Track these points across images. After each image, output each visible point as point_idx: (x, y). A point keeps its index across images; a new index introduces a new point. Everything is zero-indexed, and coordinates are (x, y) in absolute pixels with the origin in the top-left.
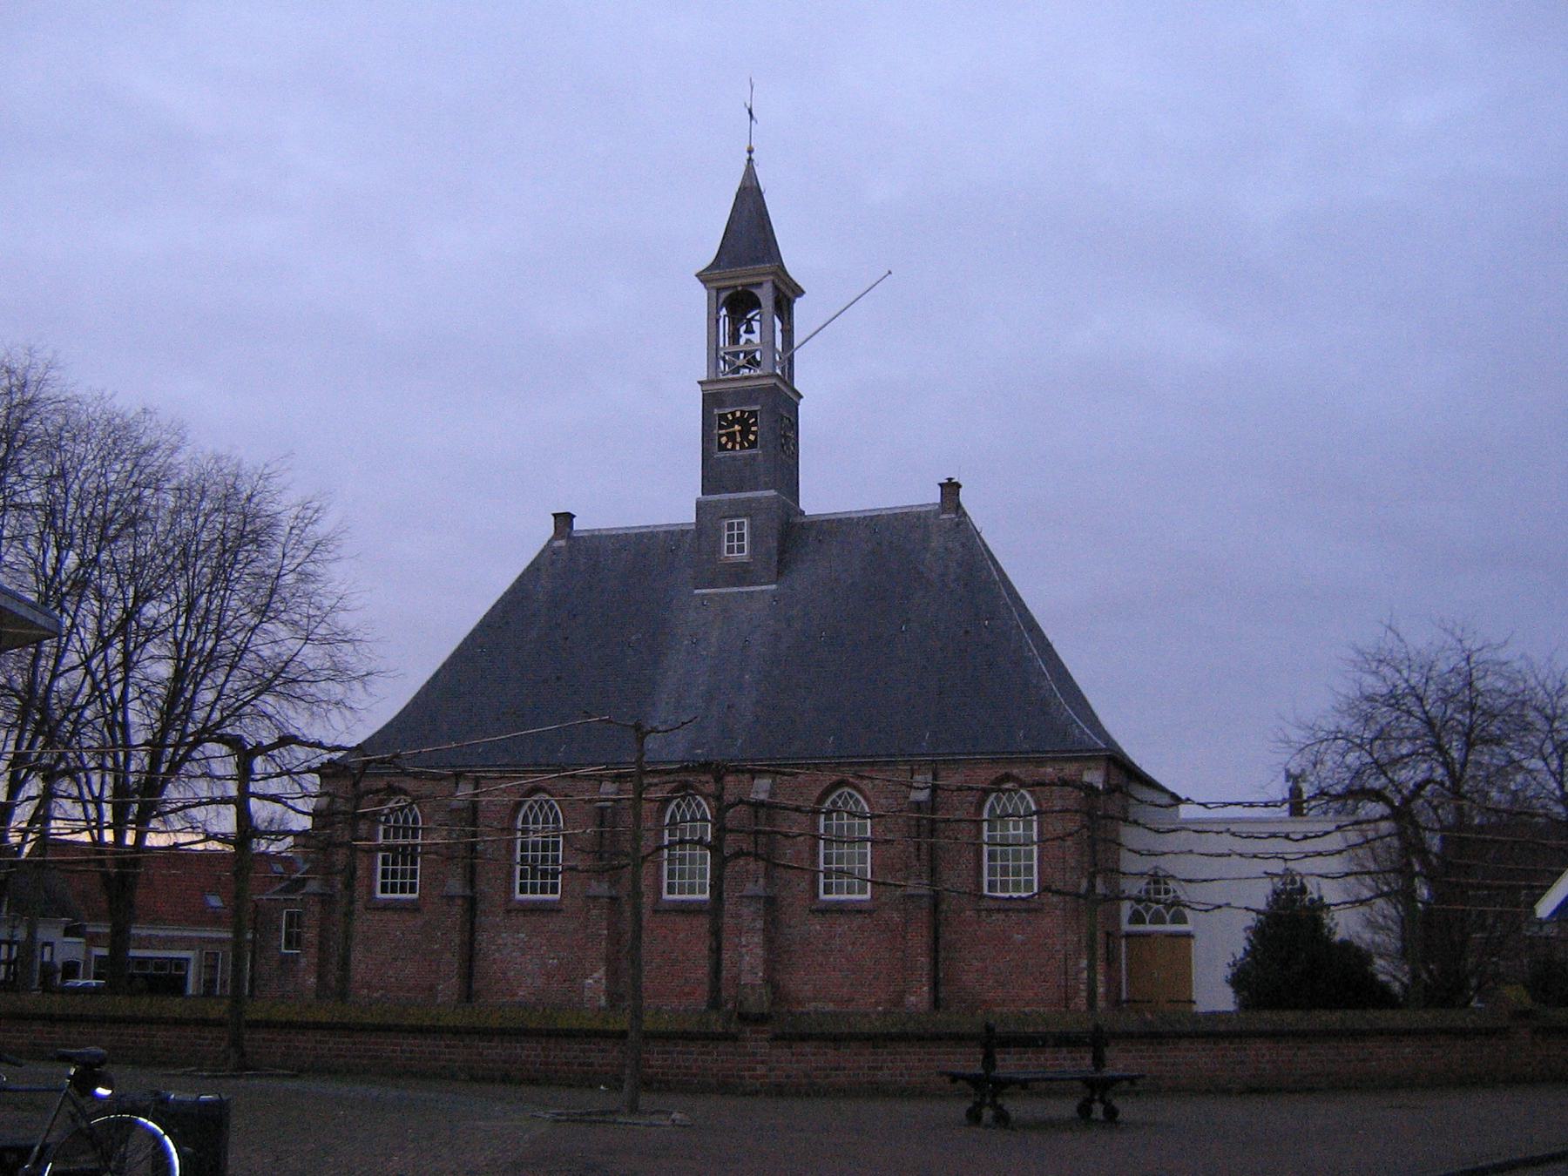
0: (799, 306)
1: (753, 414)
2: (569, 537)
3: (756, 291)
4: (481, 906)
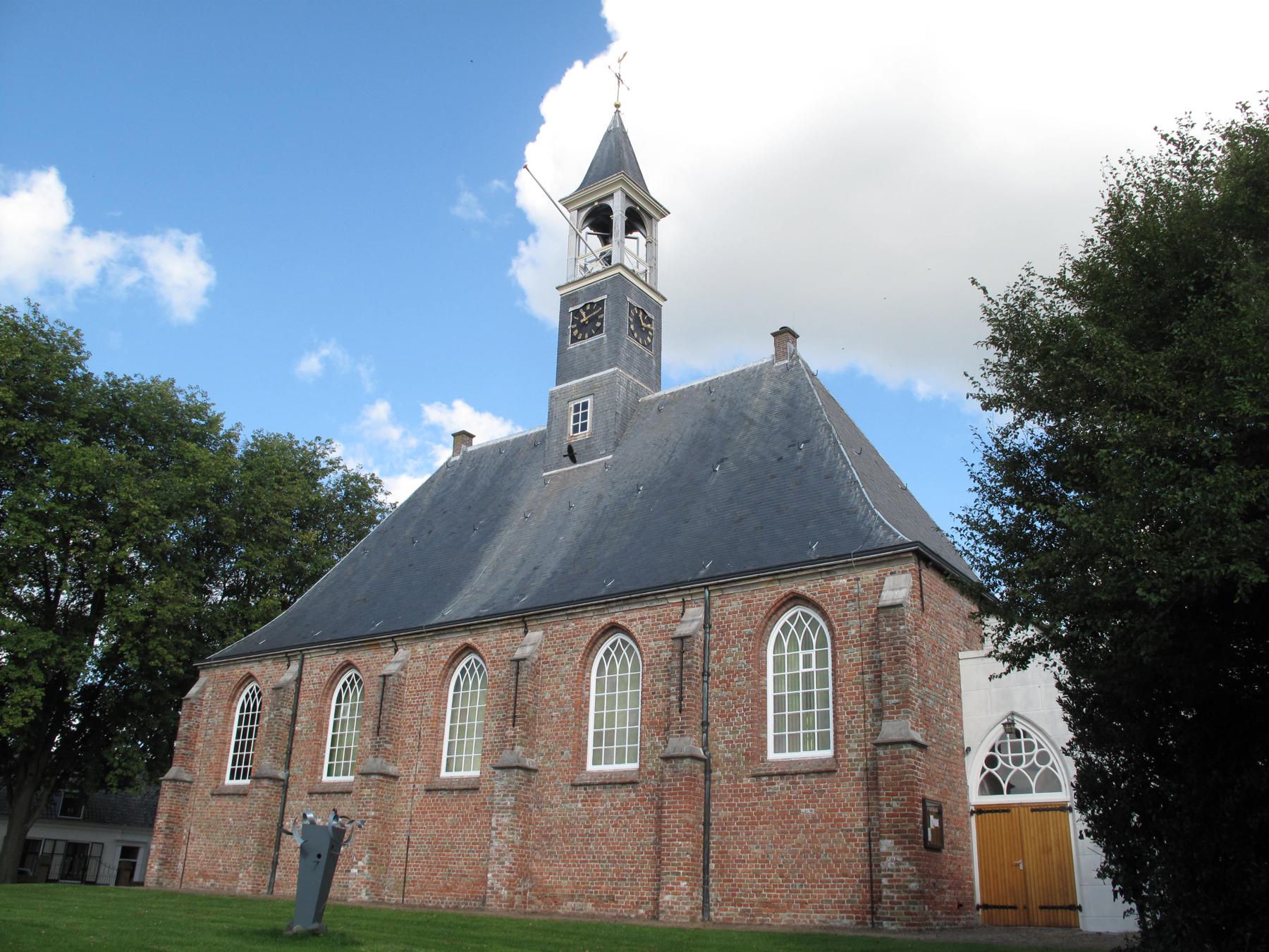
1: (601, 303)
3: (610, 203)
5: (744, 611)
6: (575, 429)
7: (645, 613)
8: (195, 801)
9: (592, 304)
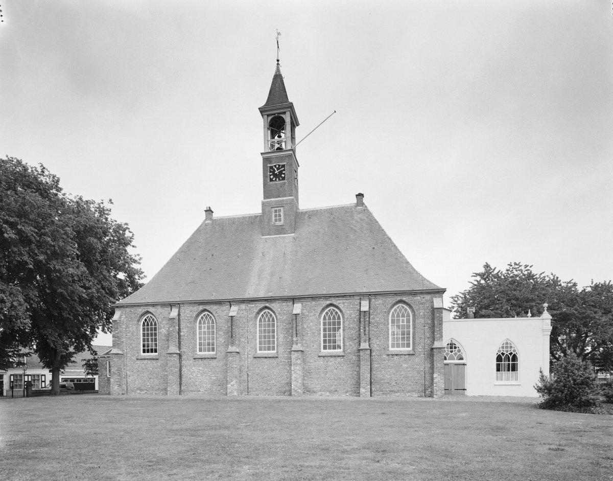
0: (297, 129)
1: (283, 166)
2: (211, 219)
4: (184, 357)
5: (383, 304)
6: (276, 220)
7: (344, 301)
9: (279, 165)
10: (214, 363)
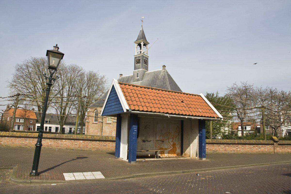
8: (90, 124)
10: (111, 125)
